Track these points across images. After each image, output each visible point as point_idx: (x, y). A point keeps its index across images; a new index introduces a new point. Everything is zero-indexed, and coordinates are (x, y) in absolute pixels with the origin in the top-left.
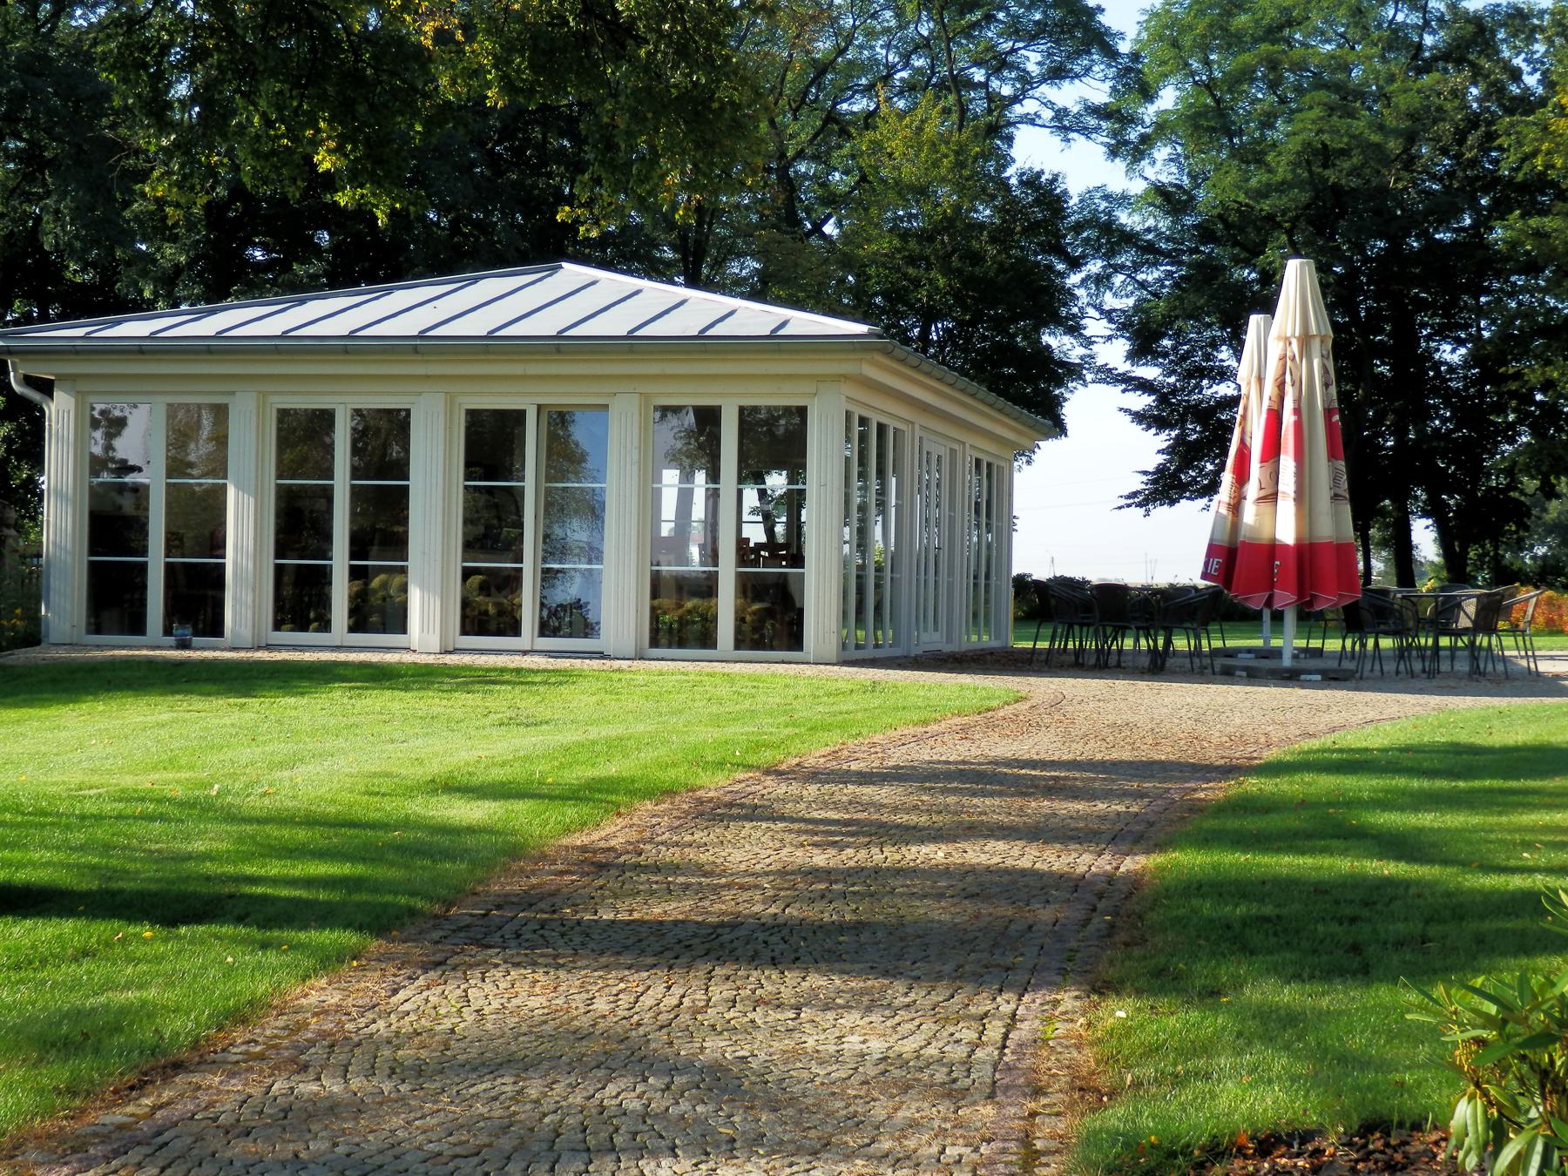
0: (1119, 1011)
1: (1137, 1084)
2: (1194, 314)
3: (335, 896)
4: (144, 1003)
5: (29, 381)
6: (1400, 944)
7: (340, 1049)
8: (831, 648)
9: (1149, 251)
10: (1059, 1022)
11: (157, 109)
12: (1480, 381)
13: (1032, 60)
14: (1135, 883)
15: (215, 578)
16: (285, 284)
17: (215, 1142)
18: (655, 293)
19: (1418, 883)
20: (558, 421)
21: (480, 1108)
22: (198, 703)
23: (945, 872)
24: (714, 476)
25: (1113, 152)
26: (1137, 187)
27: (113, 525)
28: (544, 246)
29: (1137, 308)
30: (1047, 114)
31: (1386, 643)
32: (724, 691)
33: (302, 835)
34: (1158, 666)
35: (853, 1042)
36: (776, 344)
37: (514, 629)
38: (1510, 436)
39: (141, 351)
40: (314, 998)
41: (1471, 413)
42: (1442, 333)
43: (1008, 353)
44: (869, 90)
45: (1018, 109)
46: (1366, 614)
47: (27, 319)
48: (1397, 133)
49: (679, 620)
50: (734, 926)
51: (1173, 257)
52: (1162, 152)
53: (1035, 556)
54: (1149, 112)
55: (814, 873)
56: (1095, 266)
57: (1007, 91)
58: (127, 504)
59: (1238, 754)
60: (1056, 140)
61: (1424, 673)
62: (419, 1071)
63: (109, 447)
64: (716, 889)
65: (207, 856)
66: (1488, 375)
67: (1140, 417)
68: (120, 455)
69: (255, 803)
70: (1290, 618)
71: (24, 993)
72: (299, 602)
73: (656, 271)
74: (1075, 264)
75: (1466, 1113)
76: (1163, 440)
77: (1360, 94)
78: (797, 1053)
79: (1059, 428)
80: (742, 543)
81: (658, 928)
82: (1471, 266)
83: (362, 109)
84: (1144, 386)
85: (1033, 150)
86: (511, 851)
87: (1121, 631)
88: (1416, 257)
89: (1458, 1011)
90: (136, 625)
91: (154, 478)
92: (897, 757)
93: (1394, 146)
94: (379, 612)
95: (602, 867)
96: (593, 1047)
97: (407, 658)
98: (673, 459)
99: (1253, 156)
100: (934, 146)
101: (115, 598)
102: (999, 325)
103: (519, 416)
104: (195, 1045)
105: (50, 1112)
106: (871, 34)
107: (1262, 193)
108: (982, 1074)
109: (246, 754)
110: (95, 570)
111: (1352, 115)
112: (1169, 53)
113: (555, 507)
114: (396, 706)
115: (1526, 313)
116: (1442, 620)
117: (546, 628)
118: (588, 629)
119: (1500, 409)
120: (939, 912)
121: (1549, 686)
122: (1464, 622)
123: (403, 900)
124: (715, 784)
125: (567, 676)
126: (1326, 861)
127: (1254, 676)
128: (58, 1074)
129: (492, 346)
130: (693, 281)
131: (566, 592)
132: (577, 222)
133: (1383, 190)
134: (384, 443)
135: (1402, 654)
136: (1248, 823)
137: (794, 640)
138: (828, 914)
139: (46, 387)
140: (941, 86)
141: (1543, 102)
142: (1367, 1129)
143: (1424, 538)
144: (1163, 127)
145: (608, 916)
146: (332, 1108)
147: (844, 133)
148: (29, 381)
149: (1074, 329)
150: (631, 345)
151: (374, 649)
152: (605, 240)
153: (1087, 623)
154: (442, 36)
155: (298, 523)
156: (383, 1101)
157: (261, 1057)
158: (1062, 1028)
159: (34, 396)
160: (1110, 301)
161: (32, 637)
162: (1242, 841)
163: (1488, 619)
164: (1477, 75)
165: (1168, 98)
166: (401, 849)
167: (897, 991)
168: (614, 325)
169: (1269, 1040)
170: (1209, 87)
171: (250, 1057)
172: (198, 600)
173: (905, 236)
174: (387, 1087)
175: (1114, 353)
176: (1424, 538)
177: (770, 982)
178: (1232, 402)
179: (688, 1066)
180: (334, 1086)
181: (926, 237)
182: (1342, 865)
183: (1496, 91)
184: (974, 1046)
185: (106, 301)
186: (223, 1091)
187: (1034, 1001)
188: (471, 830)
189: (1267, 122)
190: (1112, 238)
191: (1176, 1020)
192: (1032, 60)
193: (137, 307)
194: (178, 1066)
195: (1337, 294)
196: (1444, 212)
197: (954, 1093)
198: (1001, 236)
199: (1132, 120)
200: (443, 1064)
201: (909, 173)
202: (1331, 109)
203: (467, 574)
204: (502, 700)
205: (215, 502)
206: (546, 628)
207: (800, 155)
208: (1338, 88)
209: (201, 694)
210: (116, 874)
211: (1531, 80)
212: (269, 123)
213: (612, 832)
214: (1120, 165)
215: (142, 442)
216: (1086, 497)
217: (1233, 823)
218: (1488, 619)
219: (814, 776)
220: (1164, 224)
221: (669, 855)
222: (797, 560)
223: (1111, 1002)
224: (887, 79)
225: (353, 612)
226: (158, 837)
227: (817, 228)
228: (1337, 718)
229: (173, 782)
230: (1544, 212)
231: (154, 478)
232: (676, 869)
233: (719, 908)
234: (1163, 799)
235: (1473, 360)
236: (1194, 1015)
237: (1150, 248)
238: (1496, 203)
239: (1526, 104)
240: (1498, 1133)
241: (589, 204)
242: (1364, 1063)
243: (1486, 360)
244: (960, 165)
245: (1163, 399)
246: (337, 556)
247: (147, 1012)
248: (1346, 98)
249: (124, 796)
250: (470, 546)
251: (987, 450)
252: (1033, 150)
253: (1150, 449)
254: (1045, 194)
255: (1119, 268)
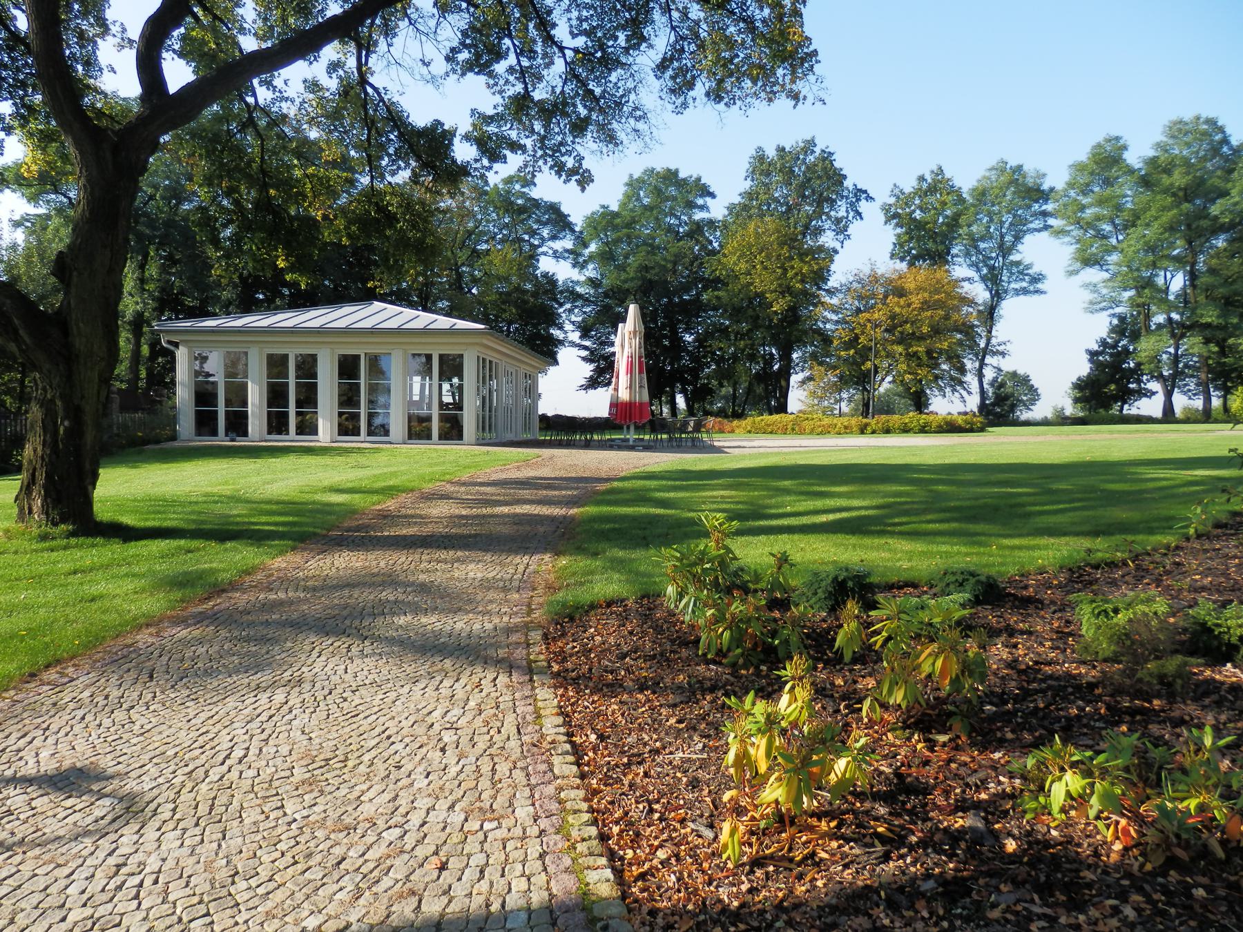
0: (563, 561)
1: (568, 585)
2: (603, 323)
3: (285, 529)
4: (211, 569)
5: (169, 342)
6: (659, 536)
7: (285, 582)
8: (473, 440)
9: (587, 301)
10: (543, 564)
11: (216, 242)
12: (698, 348)
13: (545, 233)
14: (573, 518)
15: (244, 415)
16: (270, 306)
17: (237, 616)
18: (409, 313)
19: (668, 516)
20: (374, 361)
21: (336, 601)
22: (238, 461)
23: (508, 516)
24: (431, 379)
25: (574, 266)
26: (583, 278)
27: (204, 396)
28: (368, 296)
29: (583, 321)
30: (551, 252)
31: (665, 436)
32: (434, 455)
33: (274, 507)
34: (587, 445)
35: (471, 575)
36: (451, 332)
37: (358, 434)
38: (708, 365)
39: (213, 331)
40: (276, 565)
41: (695, 358)
42: (687, 330)
43: (538, 336)
44: (486, 242)
45: (540, 250)
46: (656, 425)
47: (170, 319)
48: (670, 261)
49: (418, 429)
50: (432, 536)
51: (595, 303)
52: (591, 266)
53: (548, 406)
54: (587, 252)
55: (462, 517)
56: (568, 306)
57: (536, 243)
58: (209, 387)
59: (612, 474)
60: (554, 261)
61: (675, 446)
62: (314, 589)
63: (202, 367)
64: (426, 524)
65: (238, 516)
66: (701, 345)
67: (584, 359)
68: (206, 370)
69: (257, 496)
70: (632, 428)
71: (164, 566)
72: (277, 424)
73: (411, 305)
74: (561, 305)
75: (671, 590)
76: (592, 367)
77: (659, 248)
78: (452, 578)
79: (556, 362)
80: (441, 403)
81: (404, 537)
82: (693, 310)
83: (294, 244)
84: (586, 348)
85: (546, 264)
86: (351, 512)
87: (575, 432)
88: (677, 305)
89: (665, 559)
90: (214, 433)
91: (219, 379)
92: (494, 477)
93: (670, 266)
94: (308, 428)
95: (385, 517)
96: (379, 579)
97: (318, 444)
98: (418, 373)
99: (622, 268)
100: (511, 262)
101: (205, 423)
102: (535, 326)
103: (358, 357)
104: (230, 583)
105: (174, 608)
106: (488, 221)
107: (625, 281)
108: (516, 584)
109: (254, 479)
110: (198, 413)
111: (655, 254)
112: (593, 231)
113: (373, 389)
114: (313, 462)
115: (714, 324)
116: (683, 429)
117: (370, 433)
118: (387, 433)
119: (705, 357)
120: (505, 530)
121: (719, 450)
122: (690, 429)
123: (311, 529)
124: (428, 487)
125: (377, 450)
126: (637, 509)
127: (620, 448)
128: (178, 595)
129: (347, 332)
130: (425, 309)
131: (378, 421)
132: (376, 287)
133: (666, 281)
134: (308, 367)
135: (670, 439)
136: (614, 496)
137: (460, 436)
138: (465, 531)
139: (176, 345)
140: (513, 240)
141: (719, 252)
142: (643, 597)
143: (680, 401)
144: (591, 258)
145: (386, 534)
146: (282, 603)
147: (479, 257)
148: (169, 342)
149: (561, 328)
150: (399, 332)
151: (306, 441)
152: (392, 293)
153: (566, 430)
154: (325, 217)
155: (276, 395)
156: (300, 600)
157: (255, 586)
158: (544, 568)
159: (172, 348)
160: (573, 318)
161: (174, 438)
162: (609, 503)
163: (698, 427)
164: (697, 242)
165: (593, 247)
166: (311, 511)
167: (488, 557)
168: (393, 324)
169: (612, 569)
170: (607, 244)
171: (251, 586)
172: (238, 424)
173: (501, 293)
174: (302, 595)
175: (575, 336)
176: (680, 401)
177: (443, 554)
178: (614, 354)
179: (413, 584)
180: (282, 595)
181: (508, 294)
182: (643, 510)
183: (703, 248)
184: (514, 574)
185: (202, 312)
186: (240, 599)
187: (536, 557)
188: (338, 504)
189: (626, 257)
190: (574, 296)
191: (583, 563)
192: (545, 233)
193: (214, 315)
194: (224, 591)
195: (646, 317)
196: (686, 289)
197: (505, 589)
198: (535, 295)
199: (580, 255)
200: (327, 586)
201: (502, 272)
202: (648, 253)
203: (340, 414)
204: (353, 459)
205: (243, 388)
206: (370, 433)
207: (463, 264)
208: (651, 245)
209: (127, 466)
210: (203, 522)
211: (716, 245)
212: (259, 249)
213: (391, 504)
214: (577, 270)
215: (215, 365)
216: (565, 387)
217: (609, 497)
218: (698, 427)
219: (464, 484)
220: (592, 292)
221: (409, 512)
222: (461, 409)
223: (562, 558)
224: (493, 238)
225: (298, 428)
226: (219, 509)
227: (470, 291)
228: (646, 462)
229: (227, 490)
230: (719, 289)
231: (219, 379)
232: (412, 516)
233: (427, 530)
234: (585, 488)
235: (695, 340)
236: (589, 562)
237: (587, 300)
238: (703, 287)
239: (714, 252)
240: (681, 596)
241: (381, 280)
242: (644, 575)
243: (700, 341)
244: (519, 269)
245: (592, 353)
246: (290, 407)
247: (213, 571)
248: (654, 249)
249: (207, 495)
250: (341, 404)
251: (529, 370)
252: (546, 264)
253: (588, 370)
254: (550, 280)
255: (576, 307)
